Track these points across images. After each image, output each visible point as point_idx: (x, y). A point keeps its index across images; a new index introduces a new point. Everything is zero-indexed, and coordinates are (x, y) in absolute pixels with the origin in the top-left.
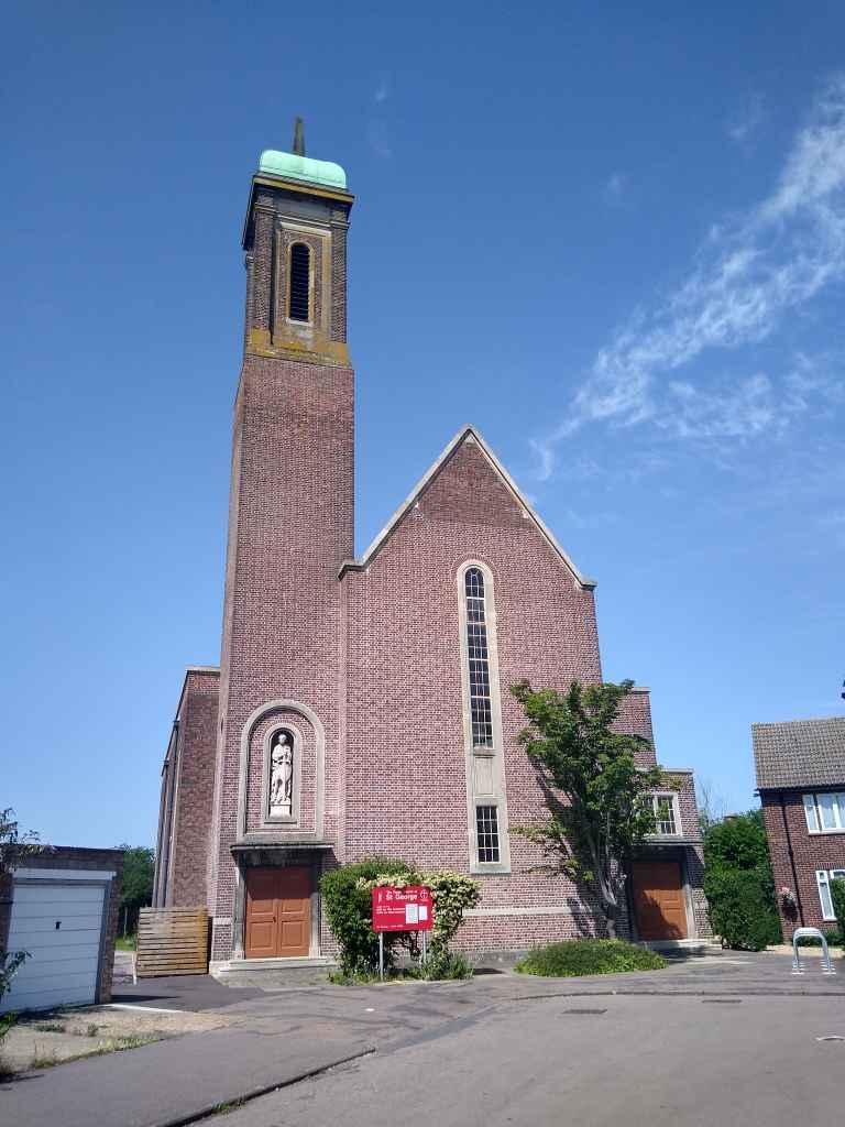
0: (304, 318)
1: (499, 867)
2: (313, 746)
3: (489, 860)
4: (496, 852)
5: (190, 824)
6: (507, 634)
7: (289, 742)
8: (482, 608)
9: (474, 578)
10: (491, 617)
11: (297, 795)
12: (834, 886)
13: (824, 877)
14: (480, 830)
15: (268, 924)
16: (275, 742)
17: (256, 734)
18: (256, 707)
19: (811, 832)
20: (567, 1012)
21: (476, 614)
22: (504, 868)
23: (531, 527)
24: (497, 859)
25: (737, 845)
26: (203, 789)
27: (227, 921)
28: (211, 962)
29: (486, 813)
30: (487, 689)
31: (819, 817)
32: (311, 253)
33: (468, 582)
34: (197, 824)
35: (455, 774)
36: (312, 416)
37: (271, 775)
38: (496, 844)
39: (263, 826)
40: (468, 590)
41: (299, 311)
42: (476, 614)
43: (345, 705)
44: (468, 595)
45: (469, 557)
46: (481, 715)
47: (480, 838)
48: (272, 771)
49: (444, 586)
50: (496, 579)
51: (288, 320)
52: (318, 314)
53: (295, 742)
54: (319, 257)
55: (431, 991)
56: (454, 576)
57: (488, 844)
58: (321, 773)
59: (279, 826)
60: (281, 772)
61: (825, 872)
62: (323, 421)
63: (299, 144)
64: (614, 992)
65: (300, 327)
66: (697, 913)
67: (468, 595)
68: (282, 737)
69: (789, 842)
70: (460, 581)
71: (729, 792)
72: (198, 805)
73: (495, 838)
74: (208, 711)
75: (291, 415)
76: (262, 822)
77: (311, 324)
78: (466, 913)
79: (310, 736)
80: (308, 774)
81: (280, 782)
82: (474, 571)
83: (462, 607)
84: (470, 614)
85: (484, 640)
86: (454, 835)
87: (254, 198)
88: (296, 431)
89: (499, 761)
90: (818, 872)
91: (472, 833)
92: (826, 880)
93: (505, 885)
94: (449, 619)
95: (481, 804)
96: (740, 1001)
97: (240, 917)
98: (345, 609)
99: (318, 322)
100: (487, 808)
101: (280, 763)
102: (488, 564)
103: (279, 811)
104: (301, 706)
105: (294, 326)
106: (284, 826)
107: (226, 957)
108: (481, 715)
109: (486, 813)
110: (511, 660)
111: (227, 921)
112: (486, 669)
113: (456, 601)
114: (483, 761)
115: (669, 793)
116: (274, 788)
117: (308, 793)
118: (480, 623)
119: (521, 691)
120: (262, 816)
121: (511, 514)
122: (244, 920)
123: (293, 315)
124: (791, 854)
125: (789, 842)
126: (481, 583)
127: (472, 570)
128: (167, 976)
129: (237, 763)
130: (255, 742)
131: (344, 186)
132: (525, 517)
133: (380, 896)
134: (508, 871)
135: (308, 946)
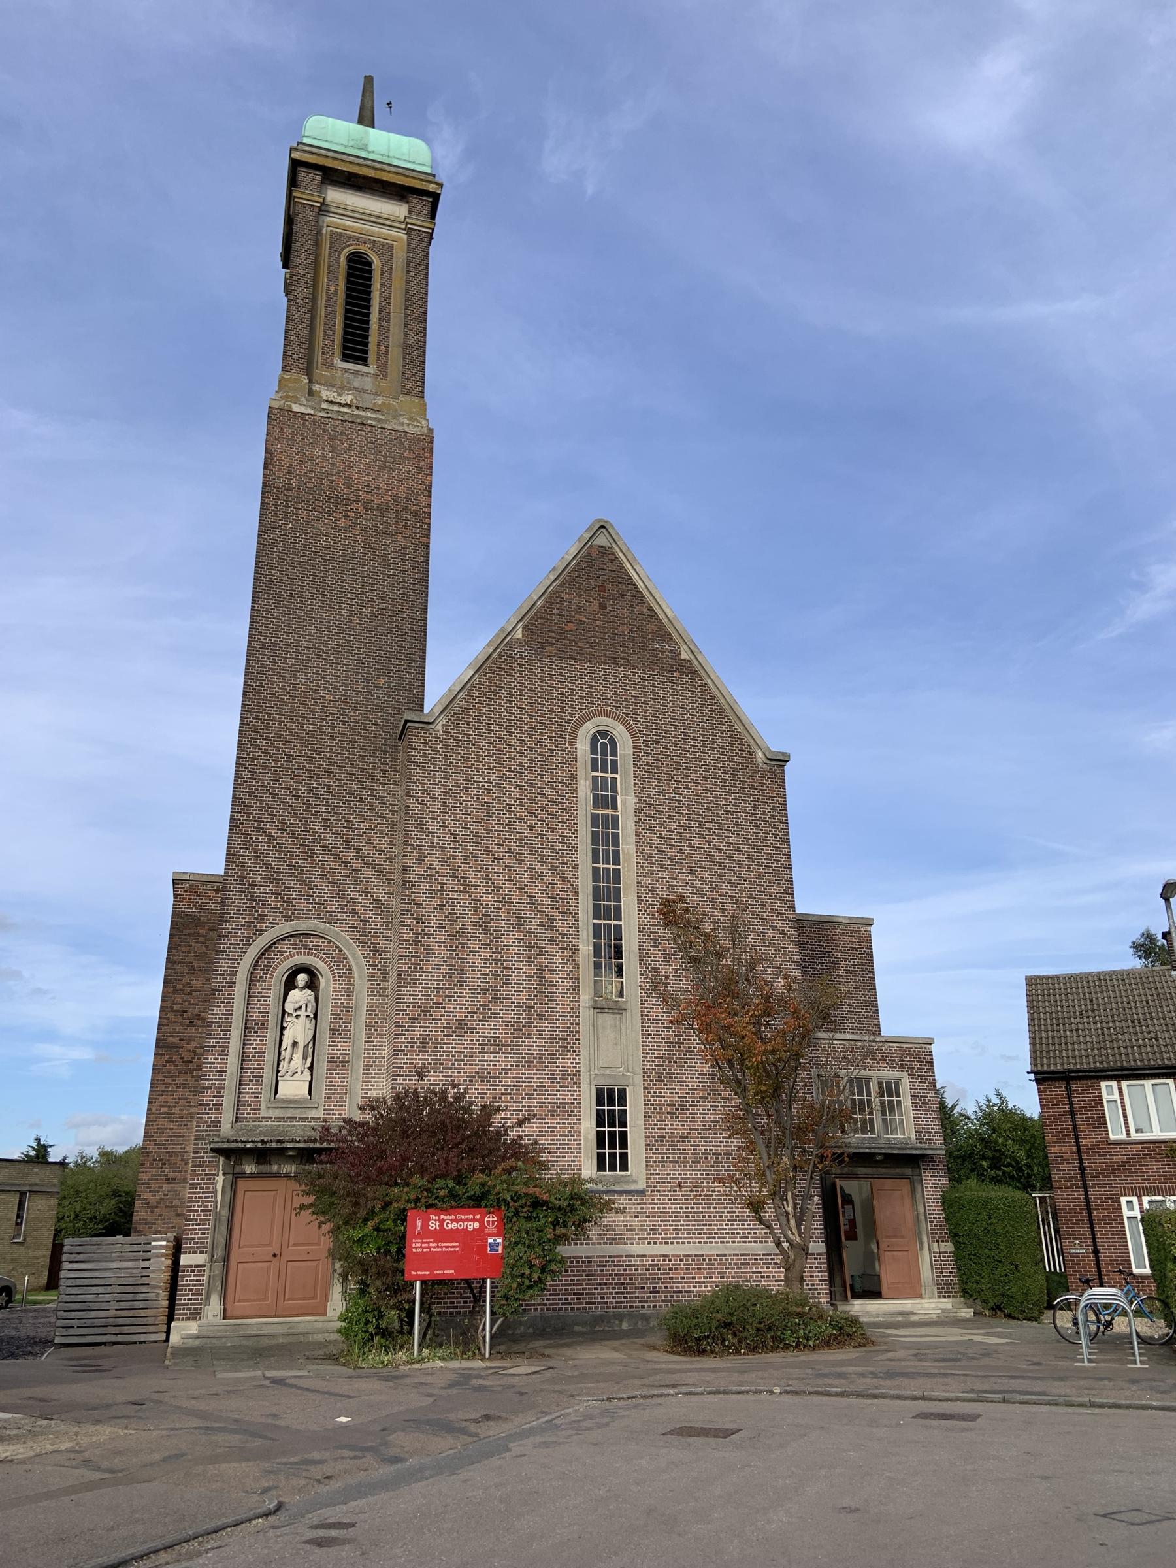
0: (364, 361)
1: (630, 1180)
2: (349, 993)
3: (613, 1168)
4: (624, 1157)
5: (164, 1110)
6: (651, 829)
7: (312, 985)
8: (614, 789)
9: (603, 745)
10: (627, 803)
11: (322, 1067)
12: (1150, 1222)
13: (1131, 1208)
14: (600, 1123)
15: (265, 1265)
16: (290, 984)
17: (259, 973)
18: (262, 932)
19: (1112, 1137)
20: (672, 1433)
21: (605, 798)
22: (636, 1182)
23: (693, 672)
24: (624, 1168)
25: (994, 1154)
26: (188, 1056)
27: (200, 1259)
28: (173, 1324)
29: (610, 1099)
30: (618, 910)
31: (1125, 1117)
32: (376, 264)
33: (594, 750)
34: (176, 1110)
35: (569, 1041)
36: (367, 502)
37: (282, 1034)
38: (624, 1145)
39: (263, 1113)
40: (594, 763)
41: (355, 347)
42: (605, 798)
43: (398, 928)
44: (594, 769)
45: (597, 714)
46: (609, 952)
47: (600, 1136)
48: (283, 1028)
49: (558, 756)
50: (636, 748)
51: (338, 362)
52: (383, 355)
53: (322, 983)
54: (387, 273)
55: (475, 1382)
56: (573, 742)
57: (612, 1145)
58: (360, 1032)
59: (290, 1113)
60: (298, 1030)
61: (1135, 1199)
62: (383, 509)
63: (367, 113)
64: (777, 1390)
65: (358, 373)
66: (938, 1258)
67: (594, 769)
68: (302, 978)
69: (1079, 1152)
70: (582, 748)
71: (987, 1067)
72: (180, 1080)
73: (624, 1135)
74: (201, 939)
75: (335, 500)
76: (263, 1106)
77: (371, 370)
78: (564, 1250)
79: (343, 972)
80: (342, 1032)
81: (295, 1044)
82: (603, 734)
83: (584, 788)
84: (595, 797)
85: (616, 837)
86: (559, 1131)
87: (293, 182)
88: (341, 524)
89: (634, 1019)
90: (1124, 1200)
91: (588, 1127)
92: (1137, 1213)
93: (636, 1209)
94: (564, 806)
95: (605, 1082)
96: (973, 1418)
97: (220, 1252)
98: (404, 786)
99: (383, 373)
100: (611, 1092)
101: (297, 1016)
102: (625, 723)
103: (293, 1087)
104: (304, 924)
105: (347, 371)
106: (298, 1113)
107: (195, 1315)
108: (609, 952)
109: (610, 1099)
110: (656, 867)
111: (200, 1259)
112: (617, 880)
113: (574, 777)
114: (608, 1019)
115: (896, 1074)
116: (286, 1055)
117: (339, 1063)
118: (610, 813)
119: (672, 914)
120: (265, 1094)
121: (663, 651)
122: (226, 1259)
123: (346, 357)
124: (1082, 1169)
125: (1079, 1152)
126: (614, 753)
127: (600, 732)
128: (105, 1344)
129: (229, 1014)
130: (259, 985)
131: (428, 171)
132: (684, 656)
133: (419, 1223)
134: (641, 1185)
135: (327, 1300)
